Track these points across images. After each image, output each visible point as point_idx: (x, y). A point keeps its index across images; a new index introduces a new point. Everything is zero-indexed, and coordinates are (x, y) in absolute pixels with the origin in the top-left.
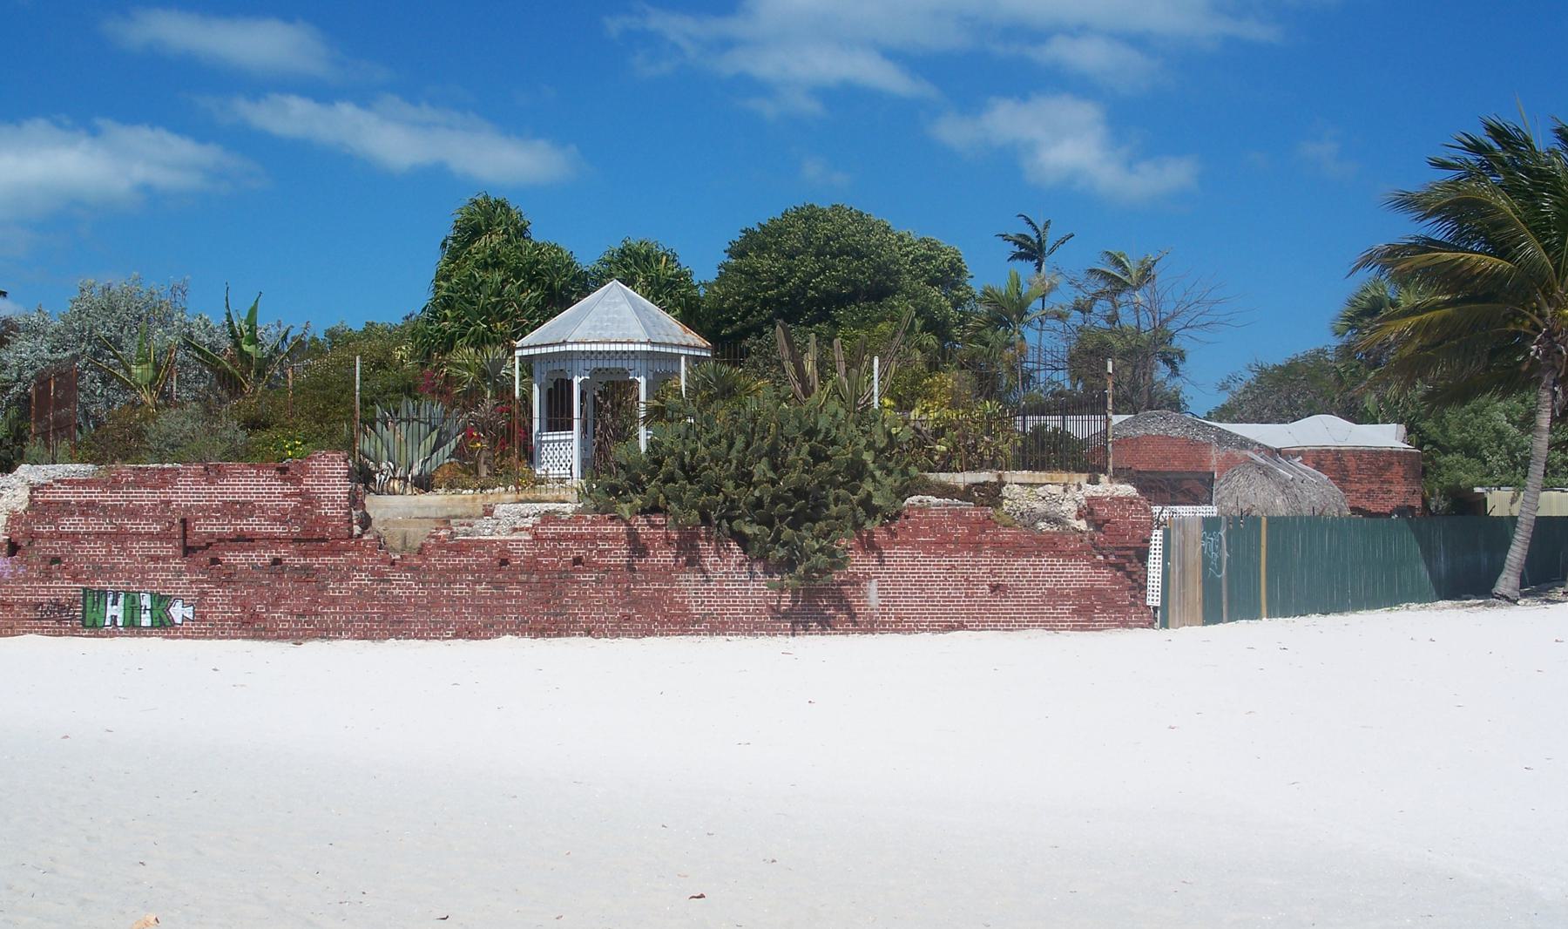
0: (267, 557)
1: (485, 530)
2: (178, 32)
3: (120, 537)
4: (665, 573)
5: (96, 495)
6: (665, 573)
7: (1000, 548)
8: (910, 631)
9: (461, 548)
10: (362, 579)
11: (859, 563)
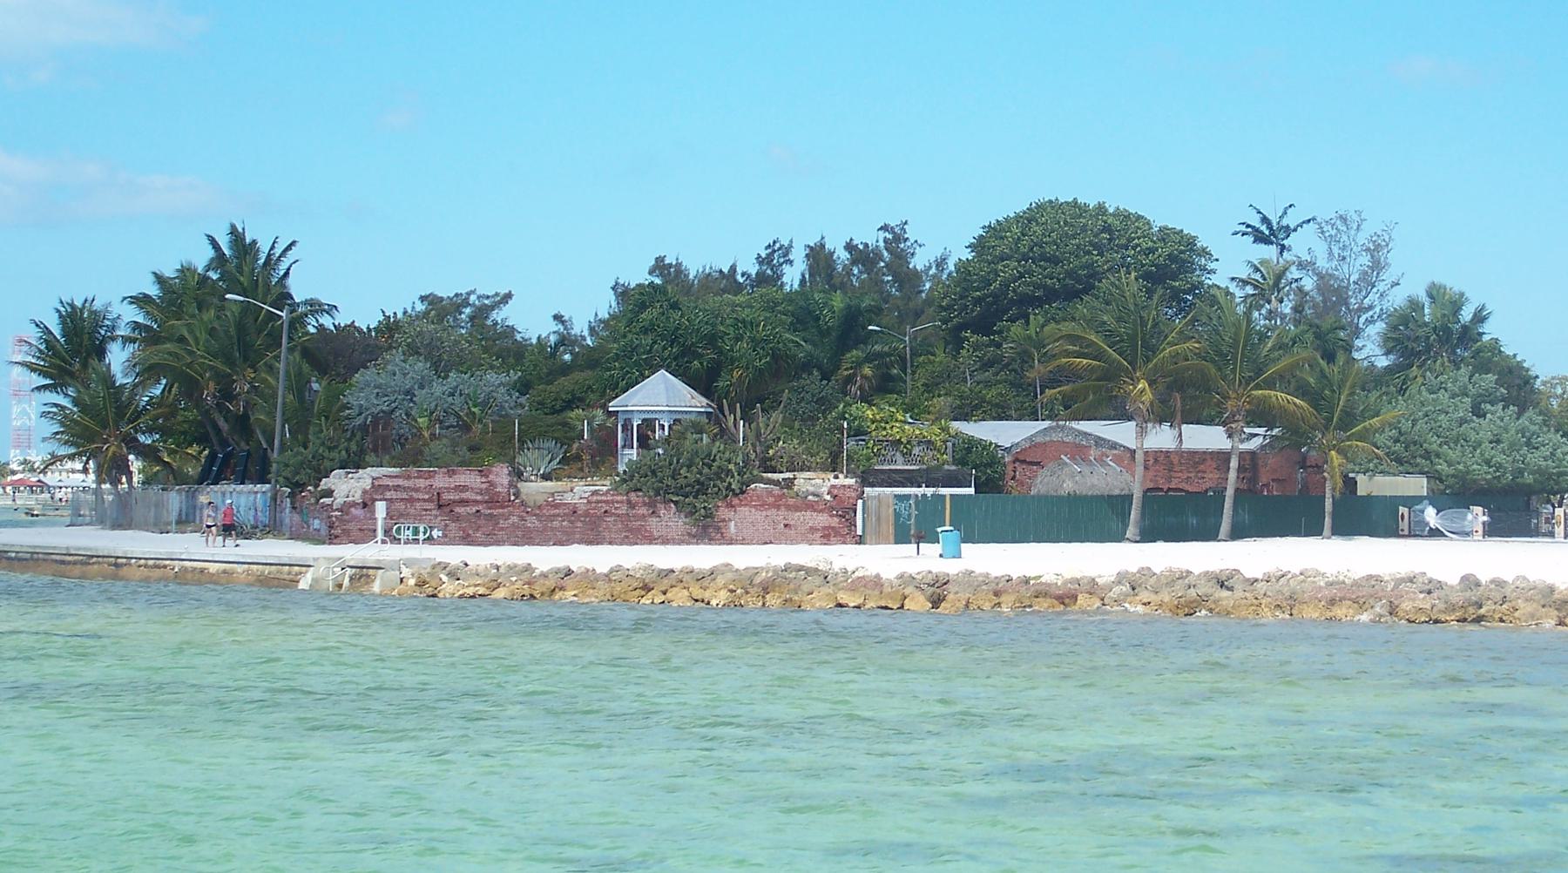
1: (569, 498)
3: (411, 500)
5: (400, 482)
7: (788, 508)
9: (556, 506)
10: (514, 519)
11: (724, 513)
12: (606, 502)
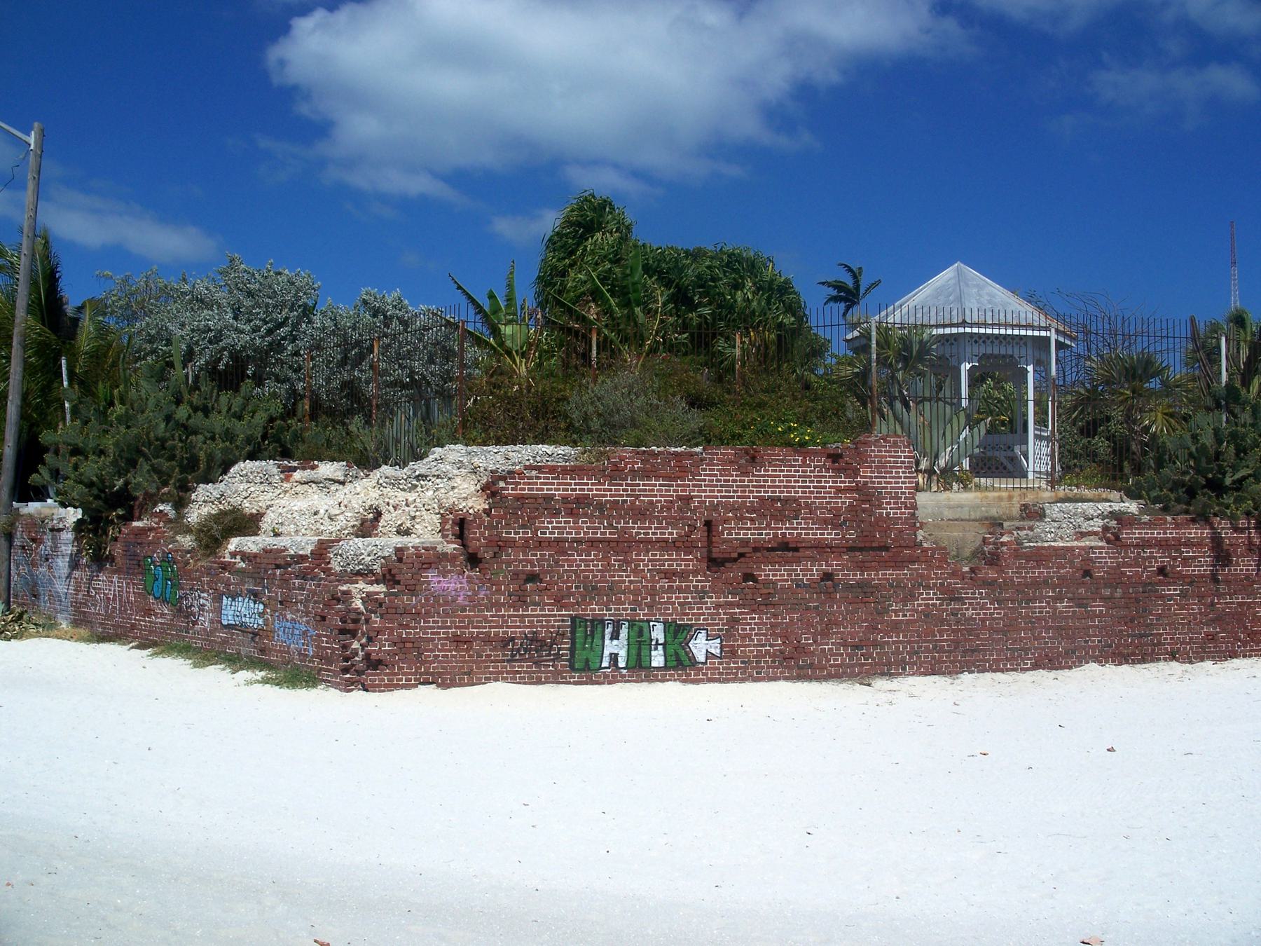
0: (816, 571)
12: (1163, 545)
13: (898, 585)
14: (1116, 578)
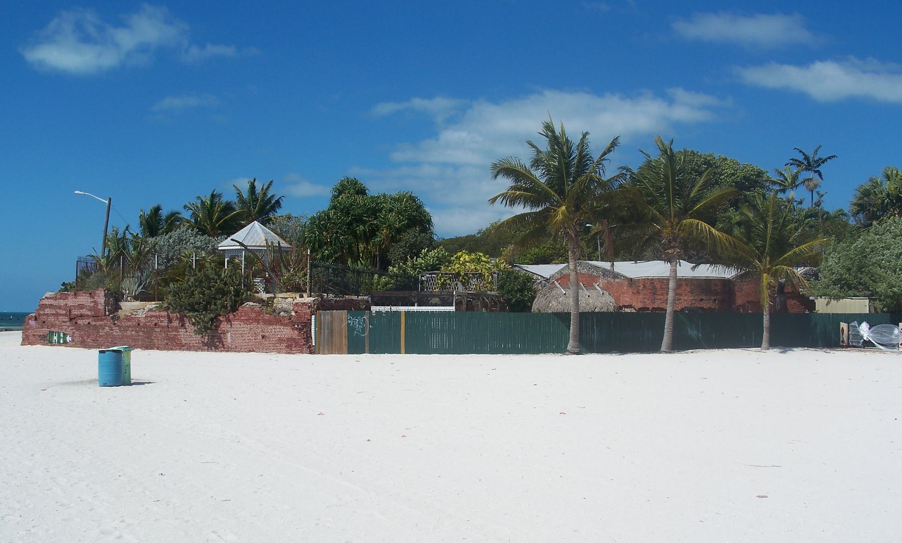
0: (88, 321)
2: (714, 28)
3: (57, 315)
4: (176, 329)
6: (176, 329)
8: (239, 352)
12: (156, 317)
13: (101, 326)
14: (145, 326)
